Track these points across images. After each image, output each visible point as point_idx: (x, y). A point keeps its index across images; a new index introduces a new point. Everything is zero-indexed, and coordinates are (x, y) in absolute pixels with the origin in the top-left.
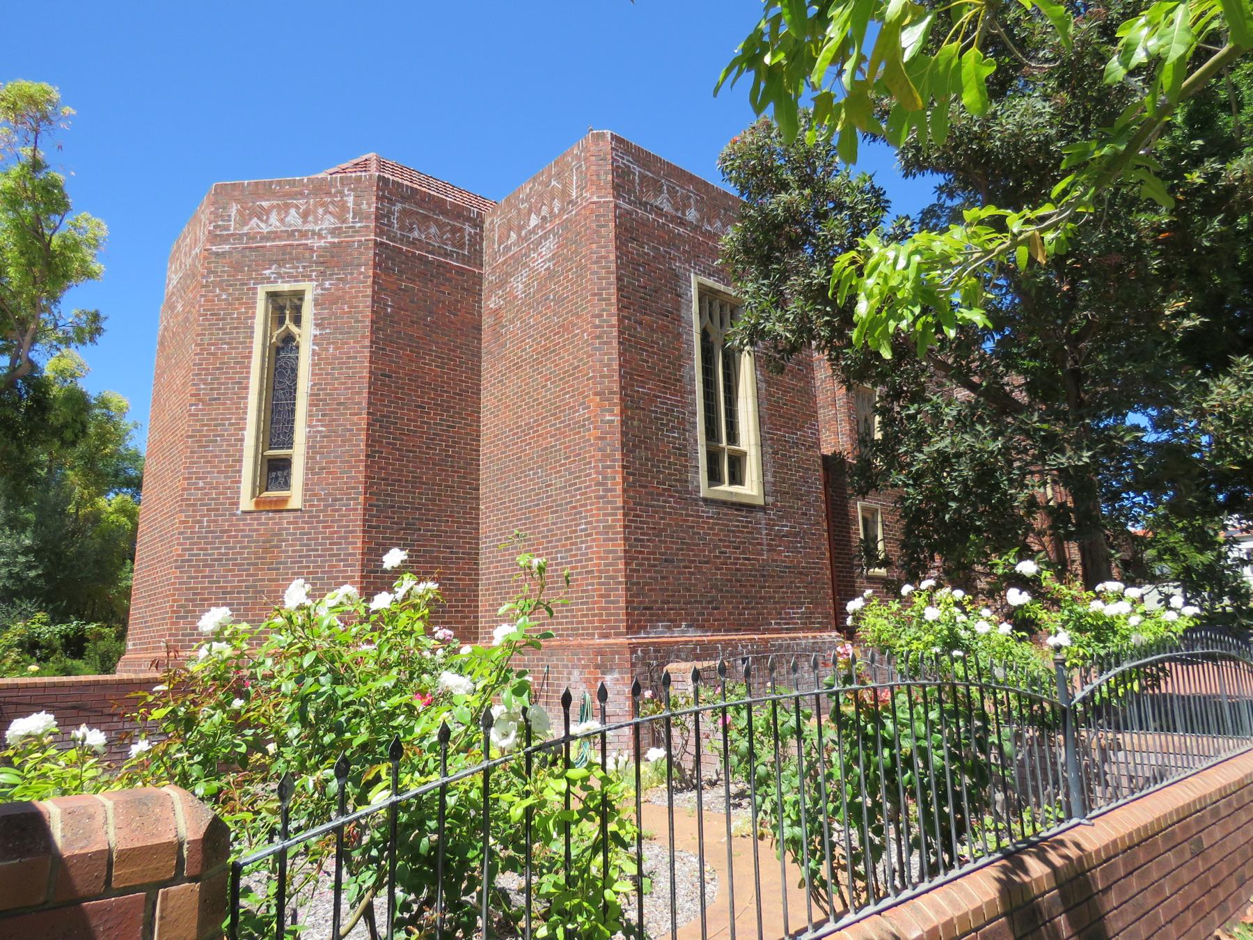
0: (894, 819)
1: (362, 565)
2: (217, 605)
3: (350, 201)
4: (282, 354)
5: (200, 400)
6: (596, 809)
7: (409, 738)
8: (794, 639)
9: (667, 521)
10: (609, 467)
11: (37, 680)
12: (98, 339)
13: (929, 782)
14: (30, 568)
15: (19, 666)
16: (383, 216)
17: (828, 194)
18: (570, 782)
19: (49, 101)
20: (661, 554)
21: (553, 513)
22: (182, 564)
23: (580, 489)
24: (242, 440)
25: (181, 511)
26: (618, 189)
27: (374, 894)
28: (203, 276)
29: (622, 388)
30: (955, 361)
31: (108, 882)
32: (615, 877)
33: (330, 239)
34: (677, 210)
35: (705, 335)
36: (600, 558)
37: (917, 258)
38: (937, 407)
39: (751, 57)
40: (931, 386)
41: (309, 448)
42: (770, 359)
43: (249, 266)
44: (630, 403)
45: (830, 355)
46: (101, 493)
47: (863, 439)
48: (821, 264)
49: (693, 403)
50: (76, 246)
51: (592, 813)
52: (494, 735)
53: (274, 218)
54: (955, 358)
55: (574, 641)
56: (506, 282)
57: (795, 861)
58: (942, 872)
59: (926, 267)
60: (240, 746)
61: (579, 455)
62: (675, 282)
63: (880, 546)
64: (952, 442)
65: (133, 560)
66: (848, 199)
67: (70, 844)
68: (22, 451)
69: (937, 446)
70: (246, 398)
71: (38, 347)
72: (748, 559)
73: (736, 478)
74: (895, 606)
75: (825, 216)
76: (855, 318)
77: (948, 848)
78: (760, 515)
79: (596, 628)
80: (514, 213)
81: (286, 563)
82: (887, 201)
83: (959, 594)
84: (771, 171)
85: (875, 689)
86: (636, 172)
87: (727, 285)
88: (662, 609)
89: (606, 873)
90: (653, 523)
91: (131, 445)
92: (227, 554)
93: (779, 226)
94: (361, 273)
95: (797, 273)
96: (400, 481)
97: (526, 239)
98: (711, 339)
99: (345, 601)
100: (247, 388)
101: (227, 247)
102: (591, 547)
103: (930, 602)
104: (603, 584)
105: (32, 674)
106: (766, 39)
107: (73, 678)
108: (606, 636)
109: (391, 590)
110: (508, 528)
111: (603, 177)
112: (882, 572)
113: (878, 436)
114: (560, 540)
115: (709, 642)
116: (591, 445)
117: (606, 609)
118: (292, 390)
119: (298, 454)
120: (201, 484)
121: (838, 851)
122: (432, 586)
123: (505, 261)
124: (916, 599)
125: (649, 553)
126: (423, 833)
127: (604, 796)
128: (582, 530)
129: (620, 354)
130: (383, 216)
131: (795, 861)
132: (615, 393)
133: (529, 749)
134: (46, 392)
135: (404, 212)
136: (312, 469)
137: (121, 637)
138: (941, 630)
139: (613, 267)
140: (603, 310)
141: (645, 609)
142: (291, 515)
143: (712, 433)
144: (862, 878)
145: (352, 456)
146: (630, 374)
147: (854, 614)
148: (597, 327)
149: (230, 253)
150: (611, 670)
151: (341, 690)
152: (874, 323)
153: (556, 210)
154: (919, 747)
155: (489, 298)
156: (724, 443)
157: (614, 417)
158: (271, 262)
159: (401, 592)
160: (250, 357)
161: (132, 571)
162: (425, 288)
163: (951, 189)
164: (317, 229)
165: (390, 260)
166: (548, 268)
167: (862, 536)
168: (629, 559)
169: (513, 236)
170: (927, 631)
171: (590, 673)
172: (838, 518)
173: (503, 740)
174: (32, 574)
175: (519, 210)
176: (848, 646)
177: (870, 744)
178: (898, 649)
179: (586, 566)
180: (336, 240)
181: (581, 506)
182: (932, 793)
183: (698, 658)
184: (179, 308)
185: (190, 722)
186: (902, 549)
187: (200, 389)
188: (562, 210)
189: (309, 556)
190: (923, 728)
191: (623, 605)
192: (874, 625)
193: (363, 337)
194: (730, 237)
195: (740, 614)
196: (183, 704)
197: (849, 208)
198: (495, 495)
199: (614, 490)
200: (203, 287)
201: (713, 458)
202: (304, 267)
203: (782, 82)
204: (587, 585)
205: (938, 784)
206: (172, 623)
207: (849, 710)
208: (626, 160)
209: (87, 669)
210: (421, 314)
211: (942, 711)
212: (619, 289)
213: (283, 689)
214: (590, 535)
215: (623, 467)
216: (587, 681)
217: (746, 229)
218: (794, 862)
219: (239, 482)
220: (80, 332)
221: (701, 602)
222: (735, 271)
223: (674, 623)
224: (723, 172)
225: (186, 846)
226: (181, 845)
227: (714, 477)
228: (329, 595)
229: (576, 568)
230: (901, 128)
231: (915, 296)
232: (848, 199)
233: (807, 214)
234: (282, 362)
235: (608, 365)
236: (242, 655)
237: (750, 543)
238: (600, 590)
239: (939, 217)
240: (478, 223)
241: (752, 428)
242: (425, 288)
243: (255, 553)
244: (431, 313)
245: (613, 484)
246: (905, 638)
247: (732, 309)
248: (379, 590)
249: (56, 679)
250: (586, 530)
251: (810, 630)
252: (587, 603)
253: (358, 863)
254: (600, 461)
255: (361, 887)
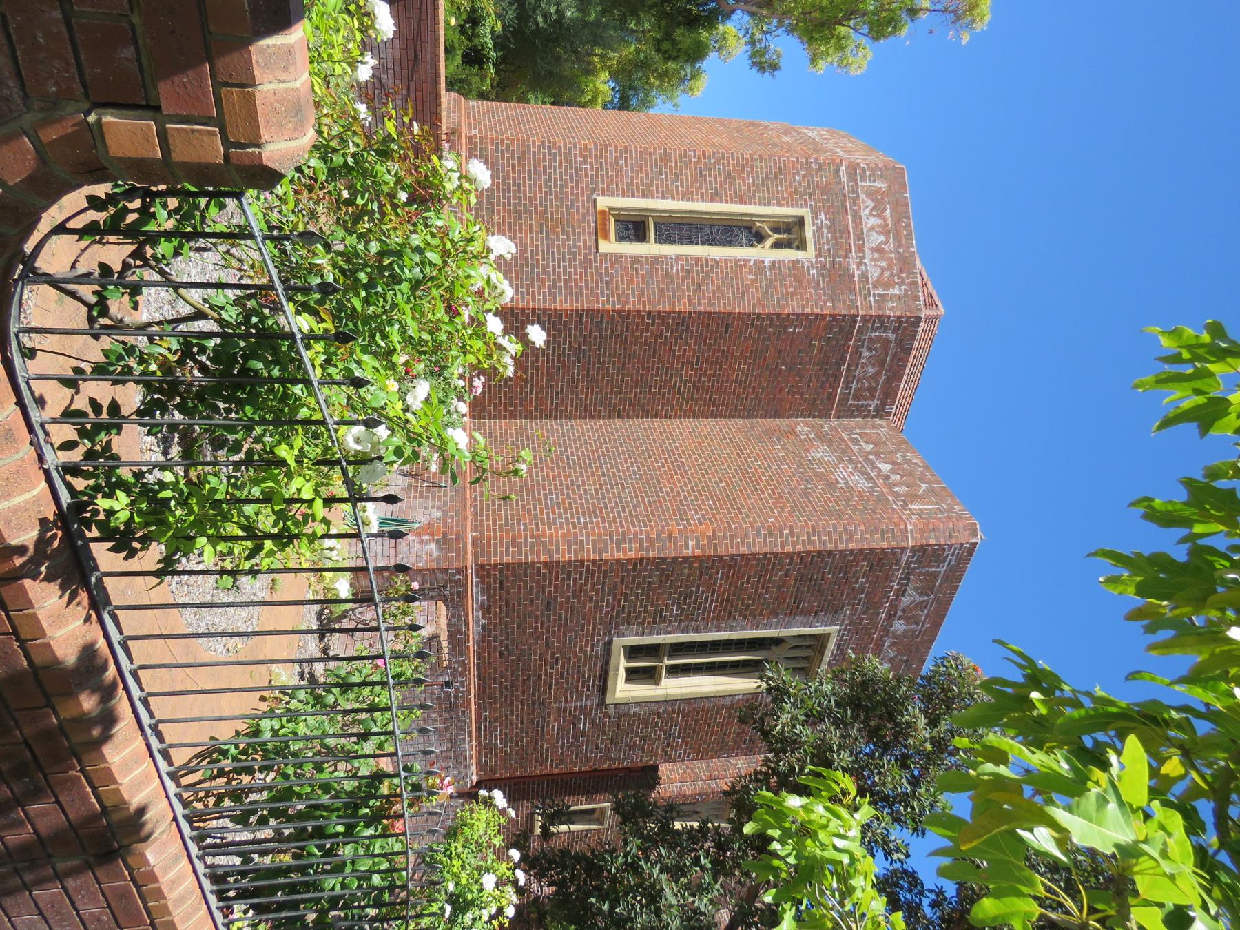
0: (279, 837)
1: (545, 310)
2: (492, 177)
3: (896, 291)
4: (745, 232)
5: (699, 159)
6: (286, 528)
7: (358, 349)
8: (470, 736)
9: (588, 604)
10: (642, 546)
11: (442, 25)
12: (754, 70)
13: (309, 874)
14: (545, 17)
15: (456, 8)
16: (882, 323)
17: (927, 769)
18: (311, 501)
19: (974, 21)
20: (556, 598)
21: (596, 490)
22: (546, 146)
23: (620, 516)
24: (663, 198)
25: (595, 145)
26: (922, 551)
27: (215, 321)
28: (816, 159)
29: (721, 557)
30: (757, 909)
31: (226, 84)
32: (219, 548)
33: (856, 273)
34: (904, 611)
35: (778, 641)
36: (551, 536)
37: (846, 860)
38: (707, 889)
39: (1037, 679)
40: (732, 882)
41: (657, 258)
42: (751, 708)
43: (827, 200)
44: (706, 566)
45: (761, 772)
46: (614, 76)
47: (673, 809)
48: (853, 762)
49: (707, 630)
50: (840, 48)
51: (281, 525)
52: (358, 430)
53: (874, 221)
54: (761, 910)
55: (470, 511)
56: (822, 442)
57: (238, 733)
58: (215, 888)
59: (839, 870)
60: (363, 198)
61: (653, 515)
62: (829, 610)
63: (564, 828)
64: (671, 906)
65: (553, 104)
66: (923, 790)
67: (262, 51)
68: (651, 7)
69: (667, 889)
70: (702, 200)
71: (747, 17)
72: (550, 688)
73: (633, 675)
74: (497, 842)
75: (905, 766)
76: (784, 794)
77: (243, 895)
78: (596, 700)
79: (482, 534)
80: (892, 448)
81: (547, 239)
82: (923, 833)
83: (510, 912)
84: (948, 708)
85: (402, 816)
86: (939, 569)
87: (830, 664)
88: (501, 599)
89: (226, 539)
90: (586, 590)
91: (659, 101)
92: (556, 186)
93: (890, 716)
94: (825, 303)
95: (842, 736)
96: (626, 343)
97: (867, 460)
98: (774, 648)
99: (498, 291)
100: (712, 201)
101: (845, 180)
102: (562, 528)
103: (499, 883)
104: (526, 540)
105: (446, 20)
106: (1058, 693)
107: (442, 55)
108: (474, 544)
109: (506, 332)
110: (581, 446)
111: (932, 535)
112: (538, 831)
113: (678, 825)
114: (569, 497)
115: (468, 648)
116: (663, 527)
117: (501, 543)
118: (711, 242)
119: (650, 248)
120: (621, 162)
121: (246, 779)
122: (510, 372)
123: (844, 440)
124: (504, 865)
125: (556, 586)
126: (267, 364)
127: (297, 536)
128: (578, 518)
129: (754, 555)
130: (882, 323)
131: (238, 733)
132: (715, 550)
133: (344, 463)
134: (704, 27)
135: (887, 342)
136: (637, 262)
137: (482, 96)
138: (472, 892)
139: (842, 547)
140: (798, 537)
141: (501, 583)
142: (593, 243)
143: (678, 649)
144: (217, 804)
145: (649, 299)
146: (735, 565)
147: (490, 798)
148: (781, 532)
149: (840, 183)
150: (441, 549)
151: (405, 286)
152: (780, 815)
153: (896, 489)
154: (344, 864)
155: (806, 424)
156: (668, 662)
157: (691, 549)
158: (832, 220)
159: (504, 342)
160: (741, 202)
161: (544, 103)
162: (815, 364)
163: (941, 904)
164: (866, 261)
165: (838, 331)
166: (838, 482)
167: (574, 808)
168: (551, 566)
169: (869, 448)
170: (470, 876)
171: (438, 528)
172: (593, 783)
173: (351, 438)
174: (540, 19)
175: (895, 453)
176: (450, 790)
177: (349, 811)
178: (453, 845)
179: (543, 524)
180: (856, 279)
181: (603, 518)
182: (295, 877)
183: (451, 636)
184: (786, 139)
185: (384, 154)
186: (560, 850)
187: (709, 158)
188: (897, 495)
189: (554, 260)
190: (363, 868)
191: (505, 560)
192: (479, 820)
193: (764, 306)
194: (877, 665)
195: (495, 679)
196: (401, 148)
197: (914, 792)
198: (613, 434)
199: (618, 551)
200: (806, 159)
201: (652, 651)
202: (829, 250)
203: (1014, 711)
204: (525, 525)
205: (306, 884)
206: (492, 140)
207: (384, 789)
208: (951, 558)
209: (452, 68)
210: (788, 360)
211: (381, 890)
212: (819, 553)
213: (414, 236)
214: (574, 527)
215: (642, 559)
216: (430, 525)
217: (886, 682)
218: (237, 731)
219: (623, 196)
220: (762, 53)
221: (507, 639)
222: (843, 672)
223: (486, 611)
224: (944, 658)
225: (257, 150)
226: (258, 146)
227: (634, 652)
228: (501, 276)
229: (542, 513)
230: (946, 828)
231: (807, 858)
232: (923, 790)
233: (905, 746)
234: (737, 232)
235: (743, 543)
236: (448, 199)
237: (566, 690)
238: (520, 537)
239: (910, 891)
240: (881, 413)
241: (684, 691)
242: (815, 364)
243: (557, 211)
244: (789, 369)
245: (624, 549)
246: (465, 853)
247: (805, 670)
248: (504, 321)
249: (442, 40)
250: (579, 522)
251: (479, 753)
252: (507, 524)
253: (245, 305)
254: (647, 536)
255: (222, 308)
